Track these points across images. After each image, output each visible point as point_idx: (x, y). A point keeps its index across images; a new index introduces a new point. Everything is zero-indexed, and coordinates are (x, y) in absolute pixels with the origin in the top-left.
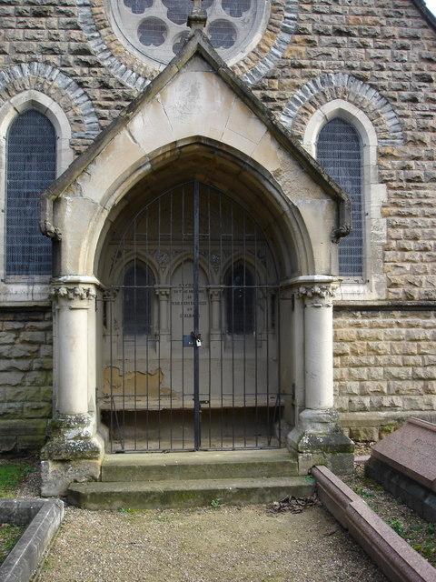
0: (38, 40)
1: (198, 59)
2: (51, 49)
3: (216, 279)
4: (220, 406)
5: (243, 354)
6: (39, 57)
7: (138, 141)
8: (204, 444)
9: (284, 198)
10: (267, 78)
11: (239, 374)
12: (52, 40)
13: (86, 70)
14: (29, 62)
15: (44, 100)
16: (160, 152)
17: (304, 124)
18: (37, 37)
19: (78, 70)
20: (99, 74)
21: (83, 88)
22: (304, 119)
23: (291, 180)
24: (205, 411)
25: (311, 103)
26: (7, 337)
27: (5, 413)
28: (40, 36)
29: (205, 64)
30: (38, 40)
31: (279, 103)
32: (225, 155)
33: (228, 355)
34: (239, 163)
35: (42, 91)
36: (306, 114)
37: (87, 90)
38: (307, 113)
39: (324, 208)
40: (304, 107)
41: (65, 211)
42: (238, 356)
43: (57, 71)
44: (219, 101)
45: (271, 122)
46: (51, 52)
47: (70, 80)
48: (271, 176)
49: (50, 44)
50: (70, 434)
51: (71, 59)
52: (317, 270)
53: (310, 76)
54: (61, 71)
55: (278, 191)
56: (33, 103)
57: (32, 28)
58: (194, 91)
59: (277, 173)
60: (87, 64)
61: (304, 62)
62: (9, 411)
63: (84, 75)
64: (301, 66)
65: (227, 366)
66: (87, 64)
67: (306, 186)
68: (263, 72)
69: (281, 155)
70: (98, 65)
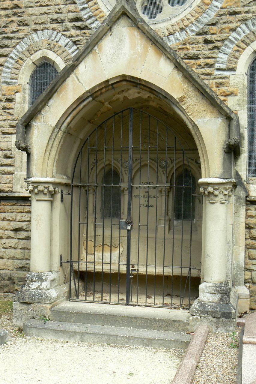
0: (47, 14)
1: (125, 17)
2: (56, 20)
3: (164, 180)
4: (179, 275)
5: (181, 236)
6: (48, 25)
7: (81, 81)
8: (134, 299)
9: (188, 118)
10: (208, 25)
11: (177, 250)
12: (57, 13)
13: (78, 32)
14: (43, 30)
15: (52, 55)
16: (97, 89)
17: (237, 58)
18: (47, 12)
19: (73, 32)
20: (87, 34)
21: (77, 45)
22: (237, 54)
23: (193, 104)
24: (135, 276)
25: (243, 41)
26: (26, 216)
27: (23, 267)
28: (49, 11)
29: (130, 21)
30: (47, 14)
31: (218, 44)
32: (145, 88)
33: (169, 236)
34: (155, 93)
35: (51, 50)
36: (238, 51)
37: (78, 46)
38: (239, 50)
39: (218, 126)
40: (237, 46)
41: (33, 133)
42: (178, 236)
43: (60, 34)
44: (139, 48)
45: (176, 60)
46: (56, 22)
47: (68, 40)
48: (177, 102)
49: (55, 16)
50: (34, 285)
51: (69, 25)
52: (211, 173)
53: (244, 21)
54: (63, 35)
55: (184, 114)
56: (45, 58)
57: (44, 6)
58: (121, 42)
59: (182, 99)
60: (79, 28)
61: (238, 9)
62: (26, 266)
63: (78, 36)
64: (235, 13)
65: (169, 246)
66: (79, 28)
67: (205, 109)
68: (205, 21)
69: (186, 86)
70: (86, 27)
